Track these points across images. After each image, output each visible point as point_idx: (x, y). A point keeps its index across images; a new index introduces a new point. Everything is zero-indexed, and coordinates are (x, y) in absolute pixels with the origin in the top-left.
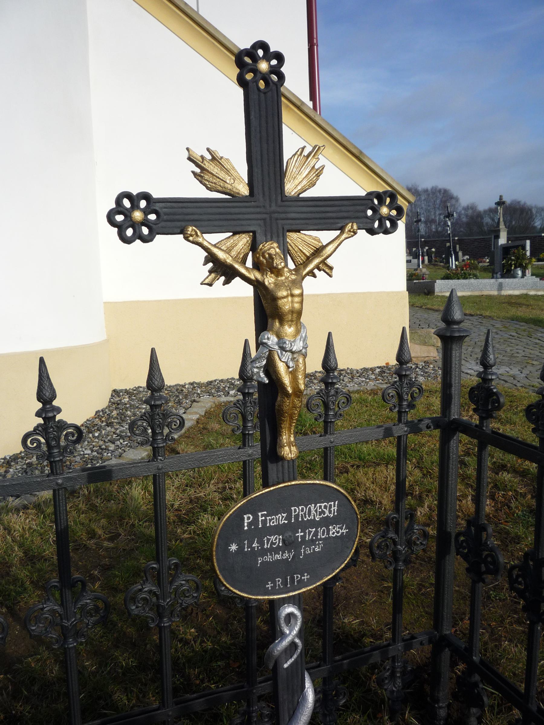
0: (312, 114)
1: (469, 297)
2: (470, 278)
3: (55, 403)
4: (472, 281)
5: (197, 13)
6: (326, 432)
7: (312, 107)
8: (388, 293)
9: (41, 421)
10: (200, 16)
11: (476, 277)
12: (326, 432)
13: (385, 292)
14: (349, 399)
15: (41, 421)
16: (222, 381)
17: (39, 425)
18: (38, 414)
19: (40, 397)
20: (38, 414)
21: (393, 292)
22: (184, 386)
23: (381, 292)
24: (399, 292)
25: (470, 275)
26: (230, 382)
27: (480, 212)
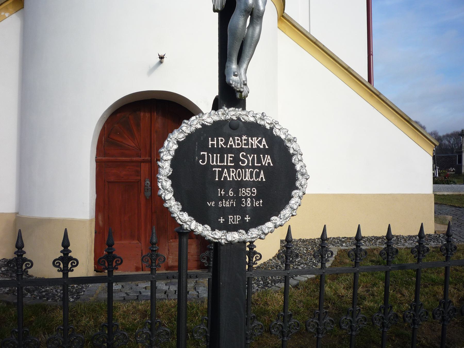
0: (368, 84)
1: (452, 195)
2: (451, 184)
3: (69, 248)
4: (453, 185)
5: (309, 33)
6: (355, 266)
7: (367, 81)
8: (423, 195)
9: (62, 255)
10: (311, 35)
11: (455, 183)
12: (355, 266)
13: (420, 194)
14: (366, 253)
15: (62, 255)
16: (334, 238)
17: (15, 258)
18: (61, 252)
19: (17, 247)
20: (61, 252)
21: (425, 194)
22: (315, 240)
23: (419, 194)
24: (429, 194)
25: (451, 181)
26: (415, 236)
27: (440, 137)
